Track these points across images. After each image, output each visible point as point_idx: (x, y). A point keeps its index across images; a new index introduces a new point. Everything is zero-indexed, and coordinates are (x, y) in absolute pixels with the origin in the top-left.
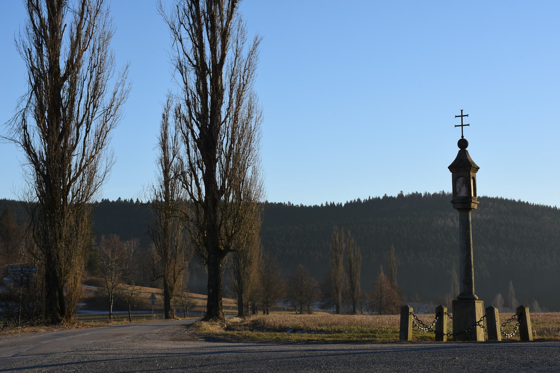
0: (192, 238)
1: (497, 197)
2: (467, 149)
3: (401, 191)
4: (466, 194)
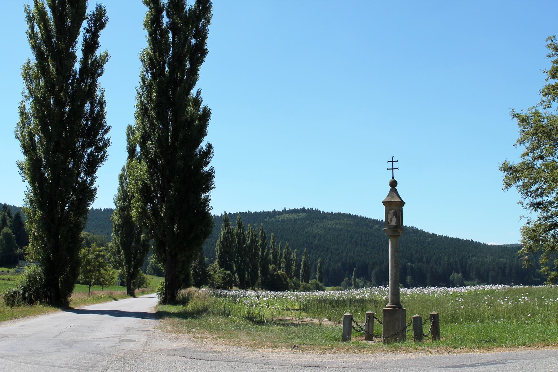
1: (361, 216)
3: (285, 207)
4: (395, 223)
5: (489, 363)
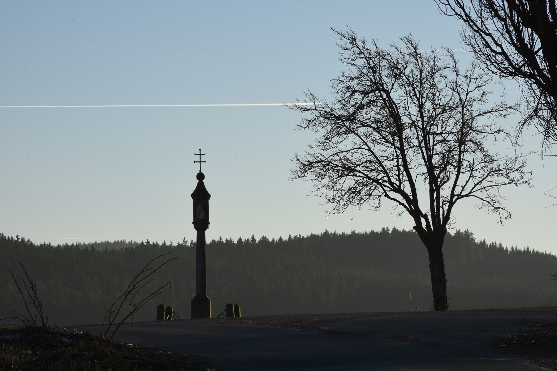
2: (203, 181)
5: (471, 22)
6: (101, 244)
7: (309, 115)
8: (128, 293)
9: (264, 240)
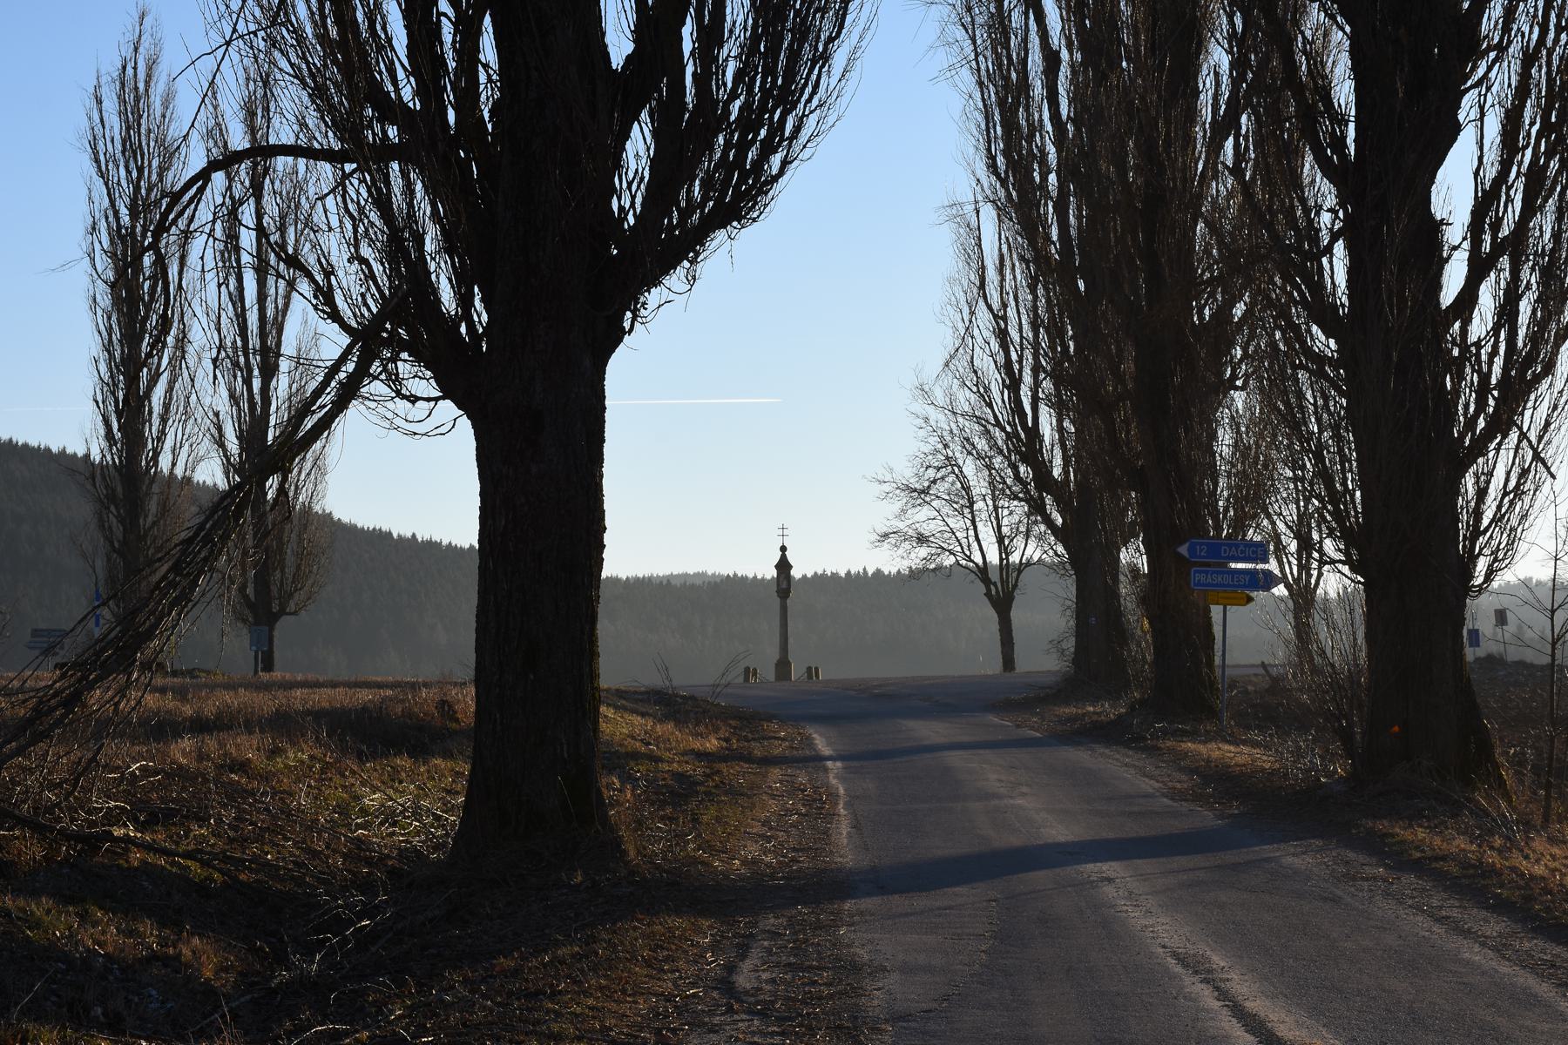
0: (1269, 516)
6: (678, 576)
7: (887, 487)
8: (724, 674)
9: (878, 572)
